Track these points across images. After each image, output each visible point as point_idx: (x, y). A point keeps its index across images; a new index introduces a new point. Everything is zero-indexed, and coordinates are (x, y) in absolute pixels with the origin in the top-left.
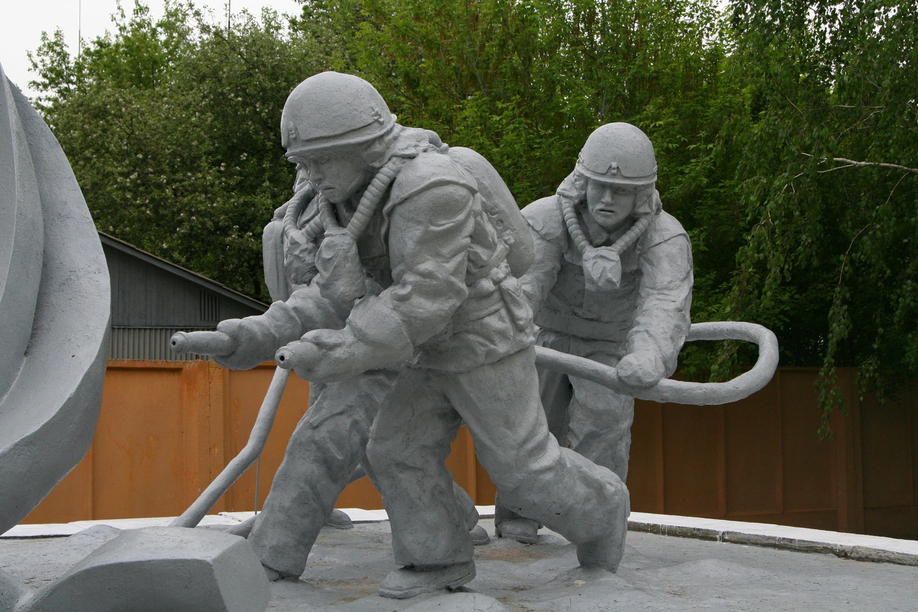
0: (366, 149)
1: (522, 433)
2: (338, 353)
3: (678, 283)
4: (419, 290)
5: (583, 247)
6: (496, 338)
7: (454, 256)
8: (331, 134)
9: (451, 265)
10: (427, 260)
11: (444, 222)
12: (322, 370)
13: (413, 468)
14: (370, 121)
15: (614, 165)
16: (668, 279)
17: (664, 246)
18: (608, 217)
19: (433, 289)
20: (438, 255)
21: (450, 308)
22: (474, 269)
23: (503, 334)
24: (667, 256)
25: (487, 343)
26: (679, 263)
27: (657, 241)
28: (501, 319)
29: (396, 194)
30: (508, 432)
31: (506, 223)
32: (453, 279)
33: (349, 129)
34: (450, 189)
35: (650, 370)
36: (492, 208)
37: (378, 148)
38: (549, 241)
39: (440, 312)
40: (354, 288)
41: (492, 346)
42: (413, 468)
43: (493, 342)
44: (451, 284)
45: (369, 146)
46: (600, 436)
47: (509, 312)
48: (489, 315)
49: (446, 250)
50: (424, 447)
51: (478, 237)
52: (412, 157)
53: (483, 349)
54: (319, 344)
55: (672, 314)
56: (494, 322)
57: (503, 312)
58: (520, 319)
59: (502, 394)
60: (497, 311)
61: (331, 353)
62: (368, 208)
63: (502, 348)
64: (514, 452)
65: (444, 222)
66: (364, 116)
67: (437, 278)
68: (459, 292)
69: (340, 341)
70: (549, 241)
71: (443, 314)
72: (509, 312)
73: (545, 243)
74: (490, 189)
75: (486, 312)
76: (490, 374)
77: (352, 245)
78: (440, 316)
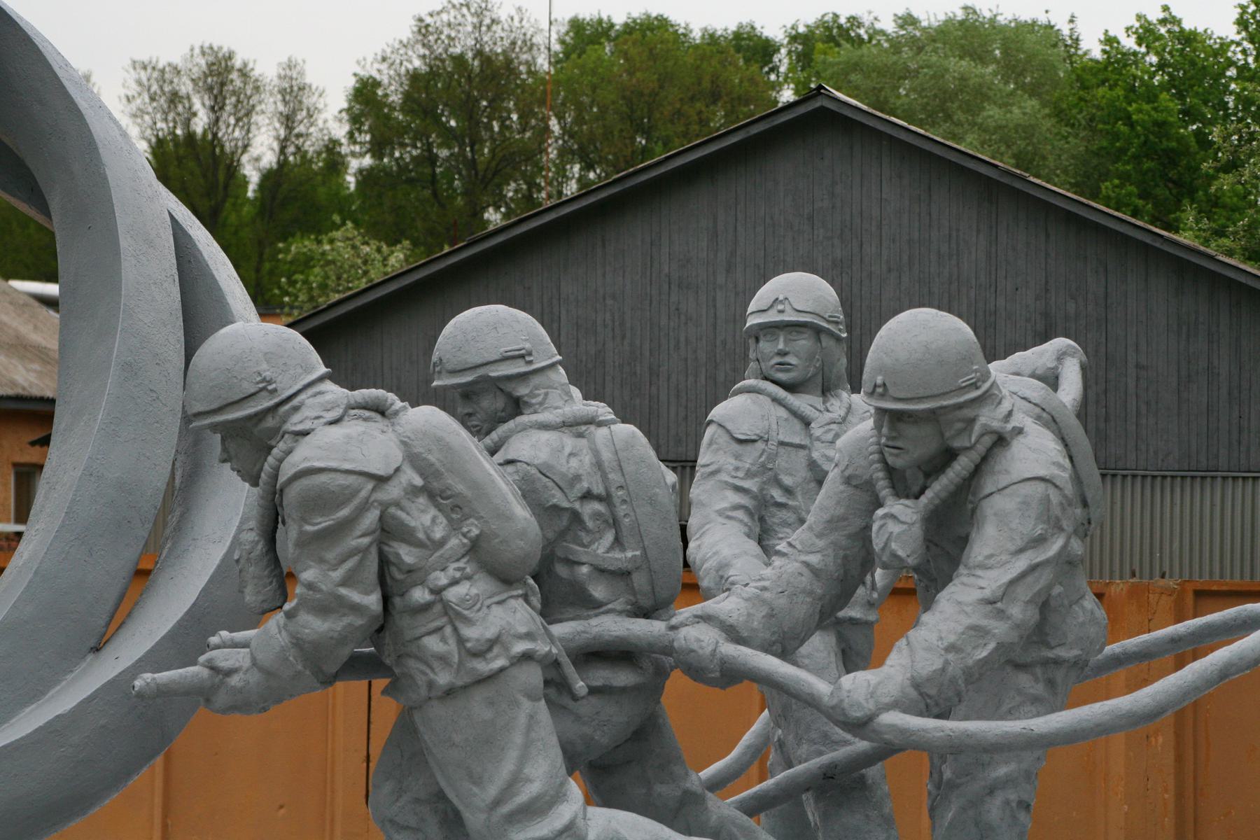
0: (256, 424)
1: (492, 791)
2: (235, 681)
3: (1004, 557)
4: (304, 603)
5: (884, 498)
6: (436, 664)
7: (343, 561)
8: (207, 409)
9: (337, 575)
10: (310, 567)
11: (320, 520)
12: (221, 699)
13: (407, 828)
14: (253, 390)
15: (879, 380)
16: (987, 552)
17: (996, 497)
18: (897, 456)
19: (328, 606)
20: (321, 561)
21: (344, 627)
22: (389, 582)
23: (443, 659)
24: (995, 514)
25: (428, 671)
26: (1013, 526)
27: (987, 491)
28: (444, 640)
29: (282, 479)
30: (475, 789)
31: (466, 510)
32: (343, 591)
33: (225, 402)
34: (323, 478)
35: (862, 700)
36: (442, 491)
37: (270, 422)
38: (856, 487)
39: (331, 634)
40: (261, 598)
41: (432, 675)
42: (407, 828)
43: (432, 670)
44: (340, 598)
45: (260, 420)
46: (958, 786)
47: (455, 630)
48: (429, 633)
49: (331, 555)
50: (417, 801)
51: (388, 530)
52: (305, 433)
53: (424, 678)
54: (213, 669)
55: (968, 609)
56: (433, 644)
57: (448, 630)
58: (468, 640)
59: (457, 738)
60: (439, 629)
61: (228, 680)
62: (837, 396)
63: (443, 678)
64: (483, 816)
65: (320, 520)
66: (245, 385)
67: (320, 591)
68: (356, 608)
69: (237, 665)
70: (856, 487)
71: (335, 635)
72: (455, 630)
73: (850, 490)
74: (438, 465)
75: (423, 630)
76: (438, 711)
77: (258, 542)
78: (332, 638)
